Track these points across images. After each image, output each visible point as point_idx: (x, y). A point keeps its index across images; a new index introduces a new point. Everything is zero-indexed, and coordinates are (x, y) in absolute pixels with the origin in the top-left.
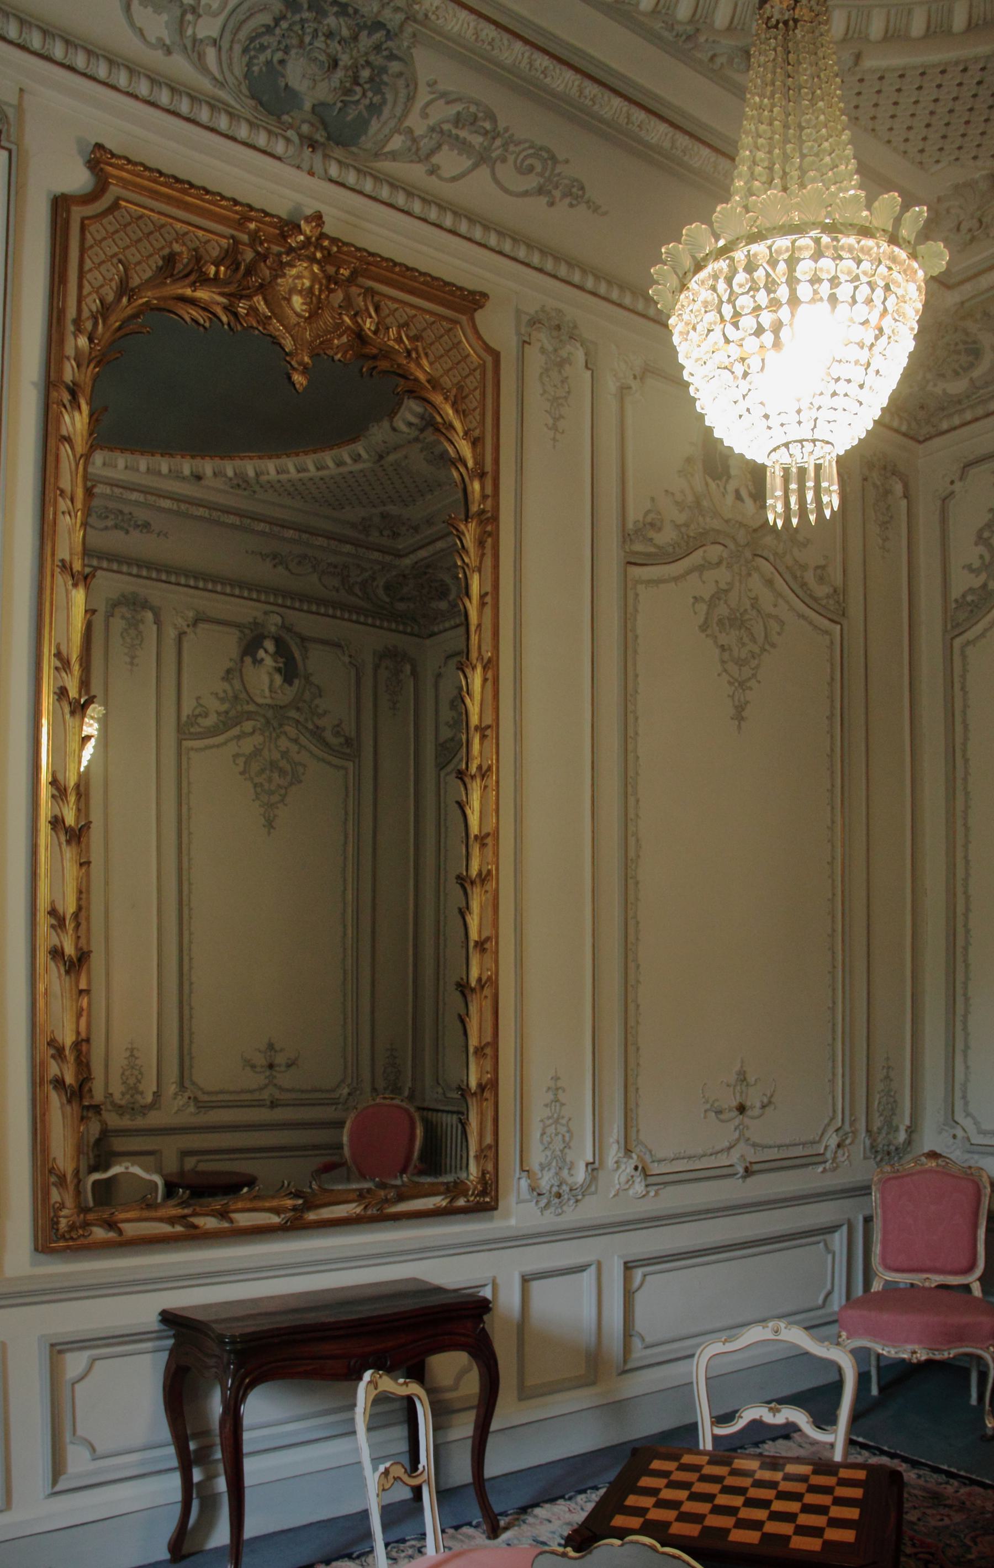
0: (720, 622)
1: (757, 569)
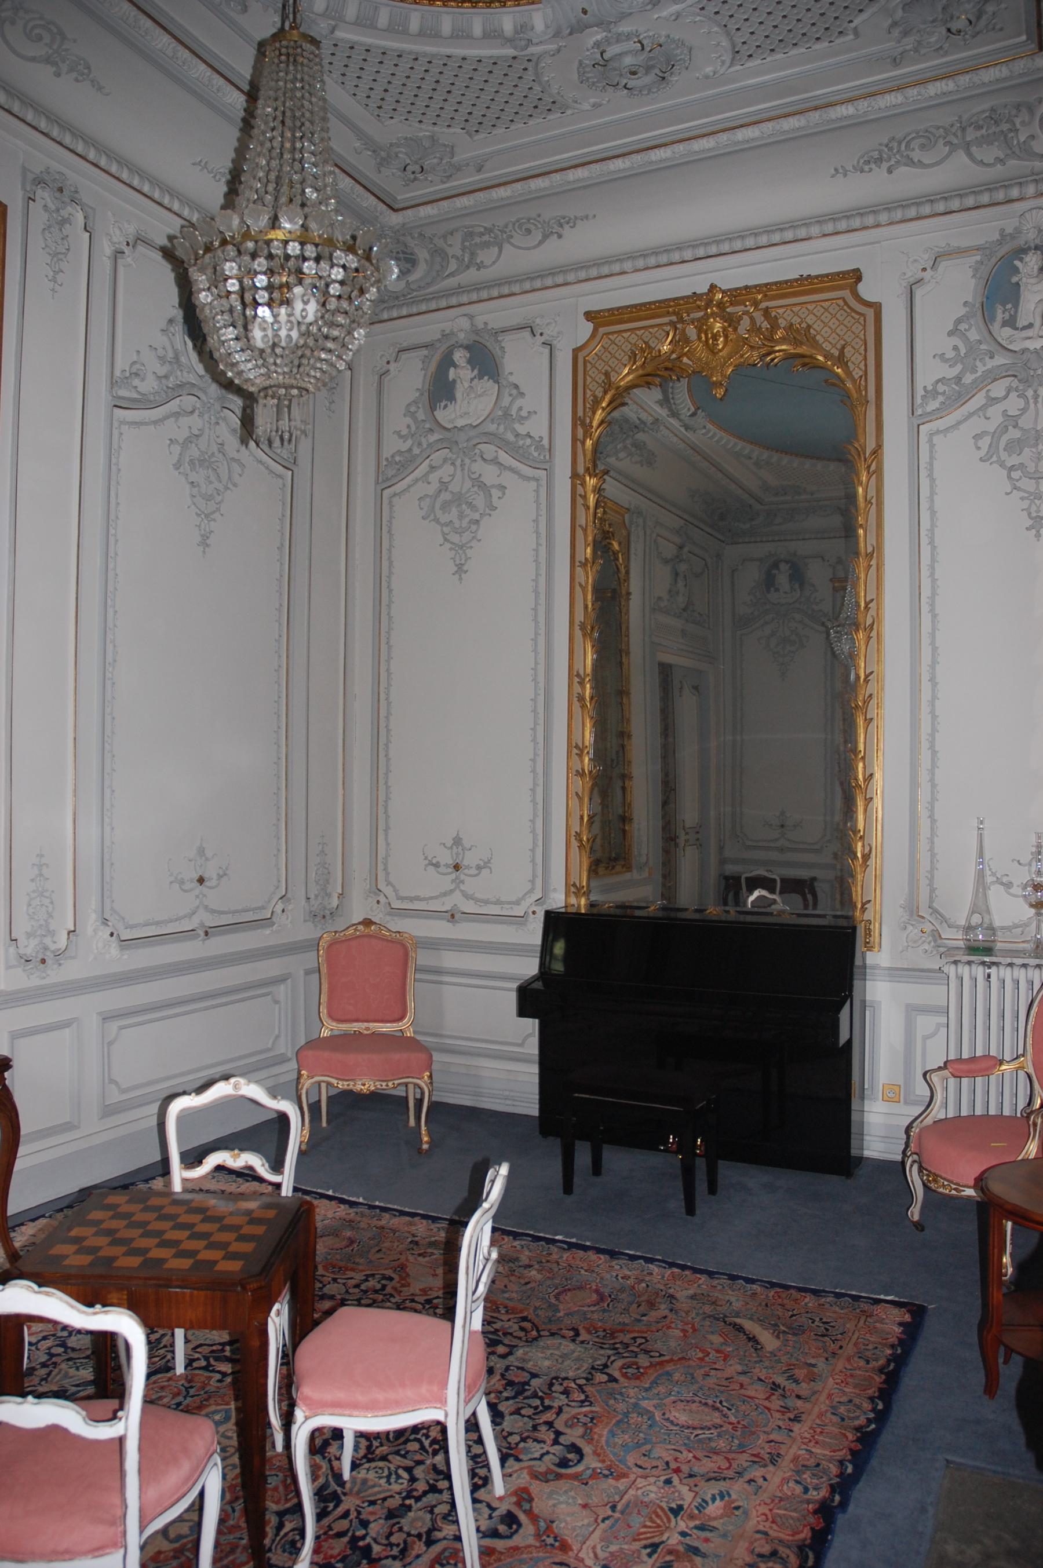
0: (192, 462)
1: (225, 419)
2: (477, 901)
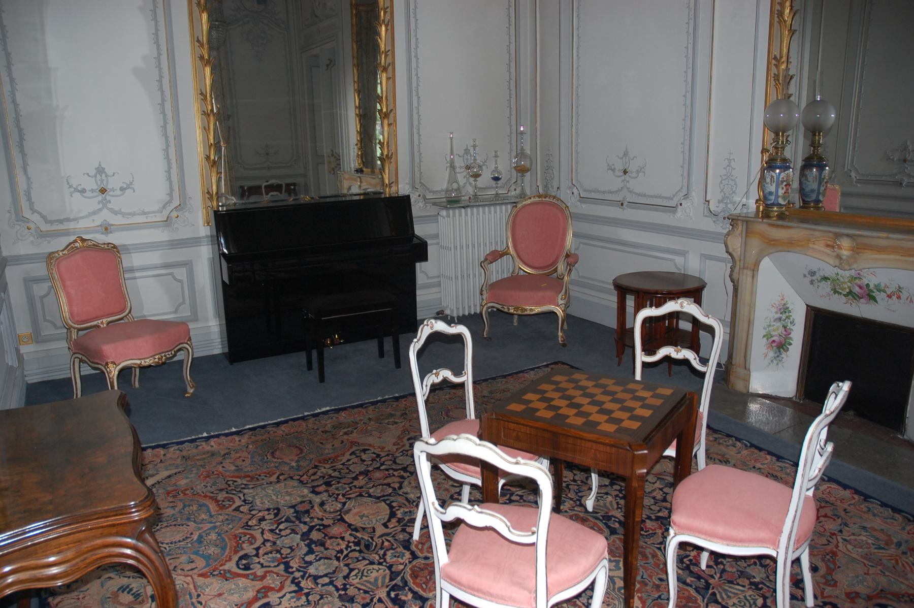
2: (124, 215)
